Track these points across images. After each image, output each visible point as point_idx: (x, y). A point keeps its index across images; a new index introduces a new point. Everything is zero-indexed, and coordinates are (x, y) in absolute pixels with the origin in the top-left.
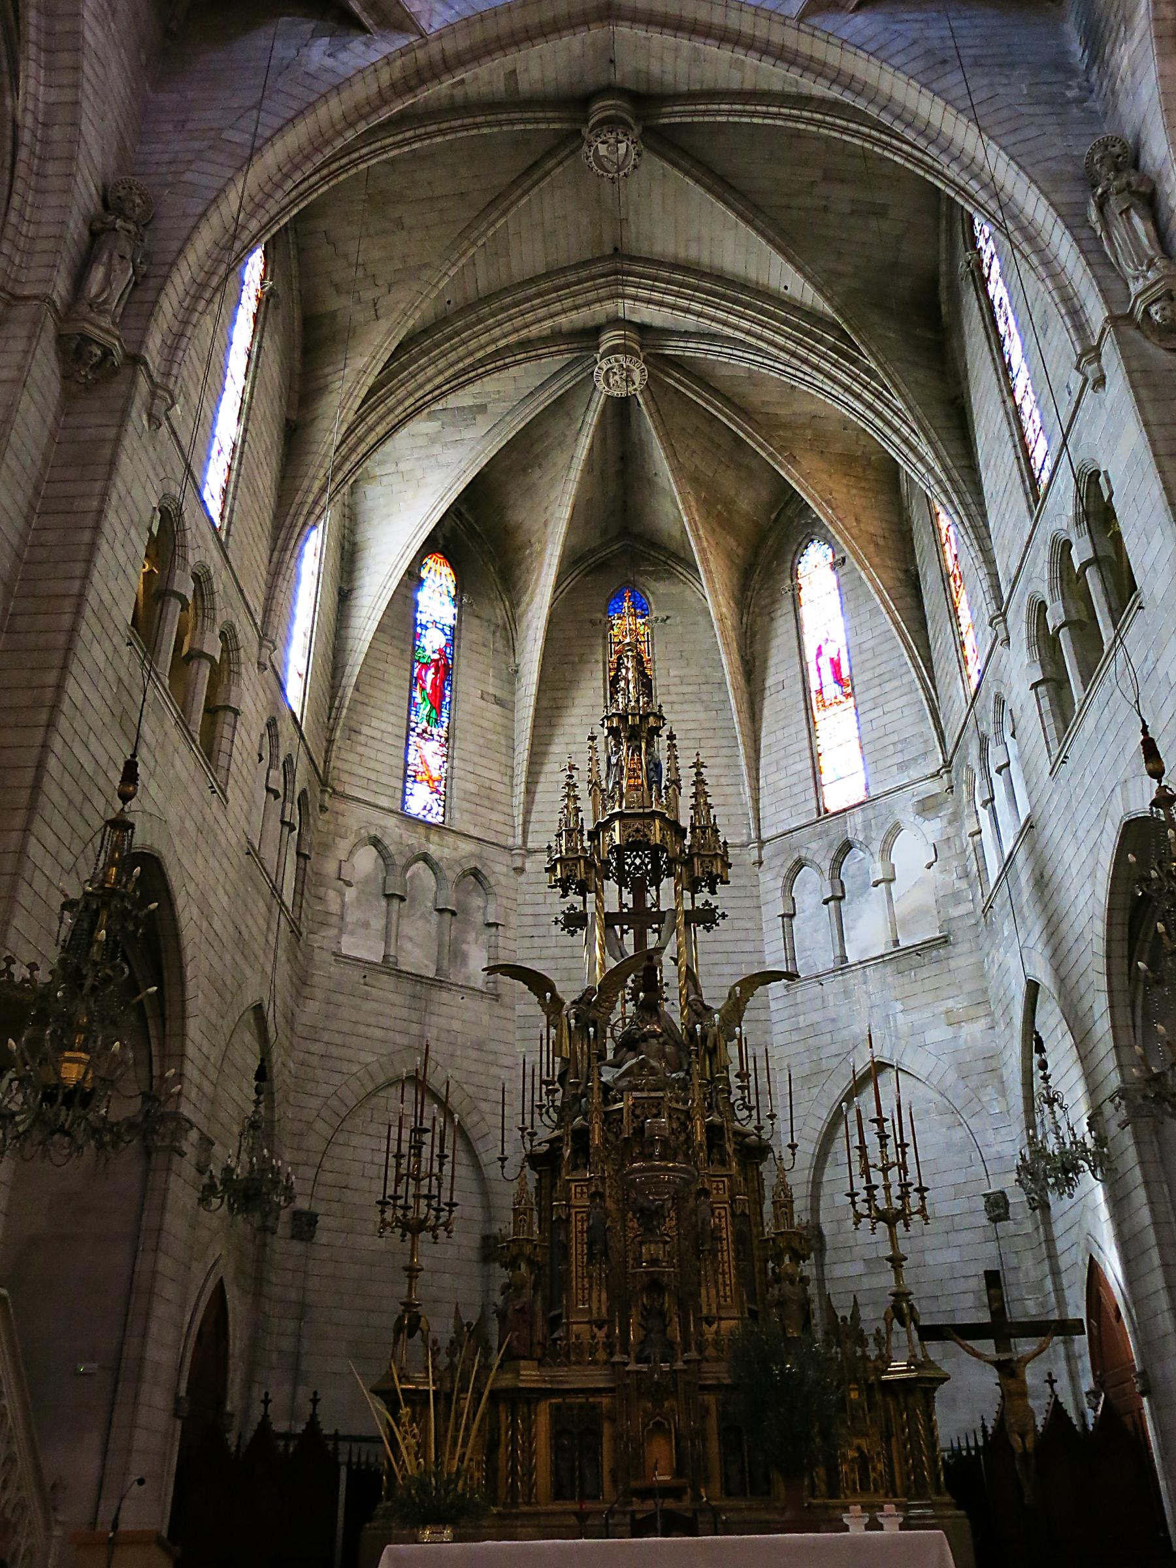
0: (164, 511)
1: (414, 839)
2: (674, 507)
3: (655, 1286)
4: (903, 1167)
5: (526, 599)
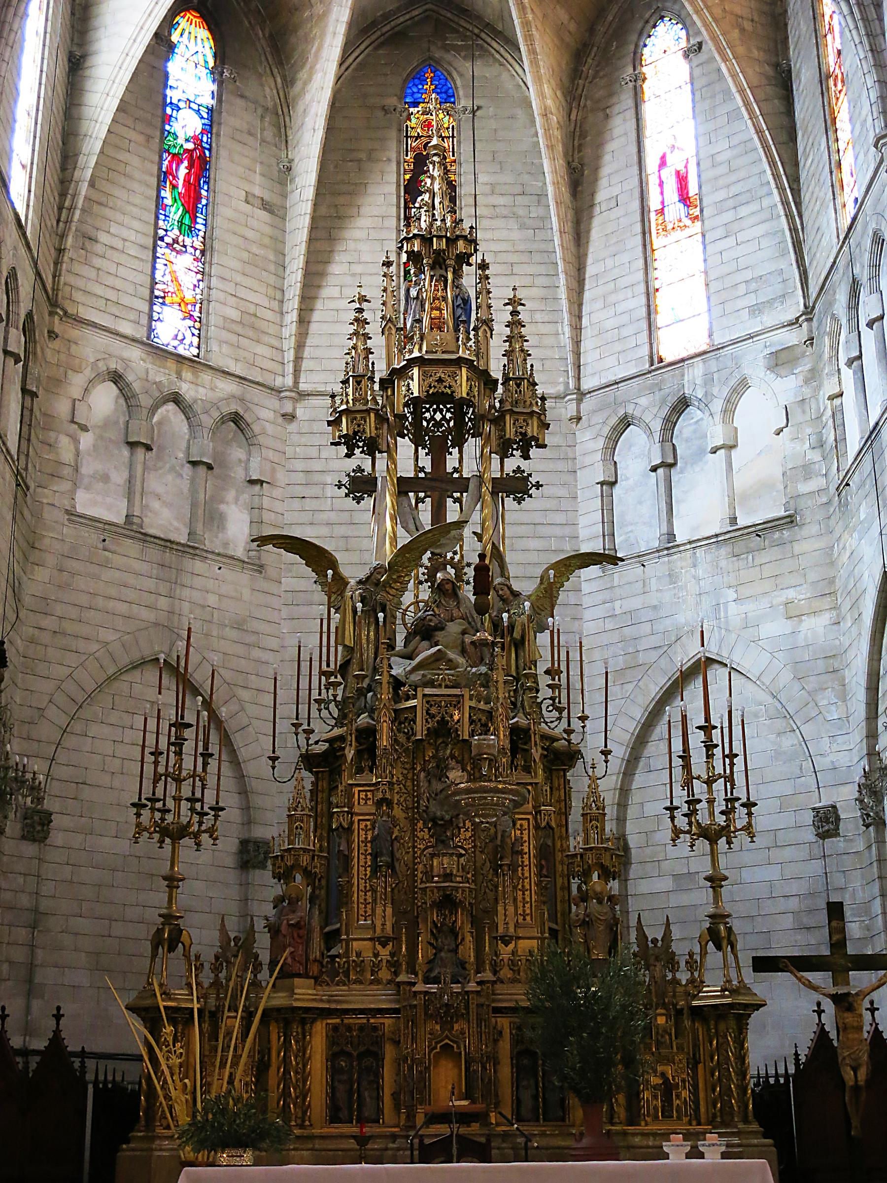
1: (163, 375)
3: (447, 902)
4: (730, 779)
5: (303, 75)
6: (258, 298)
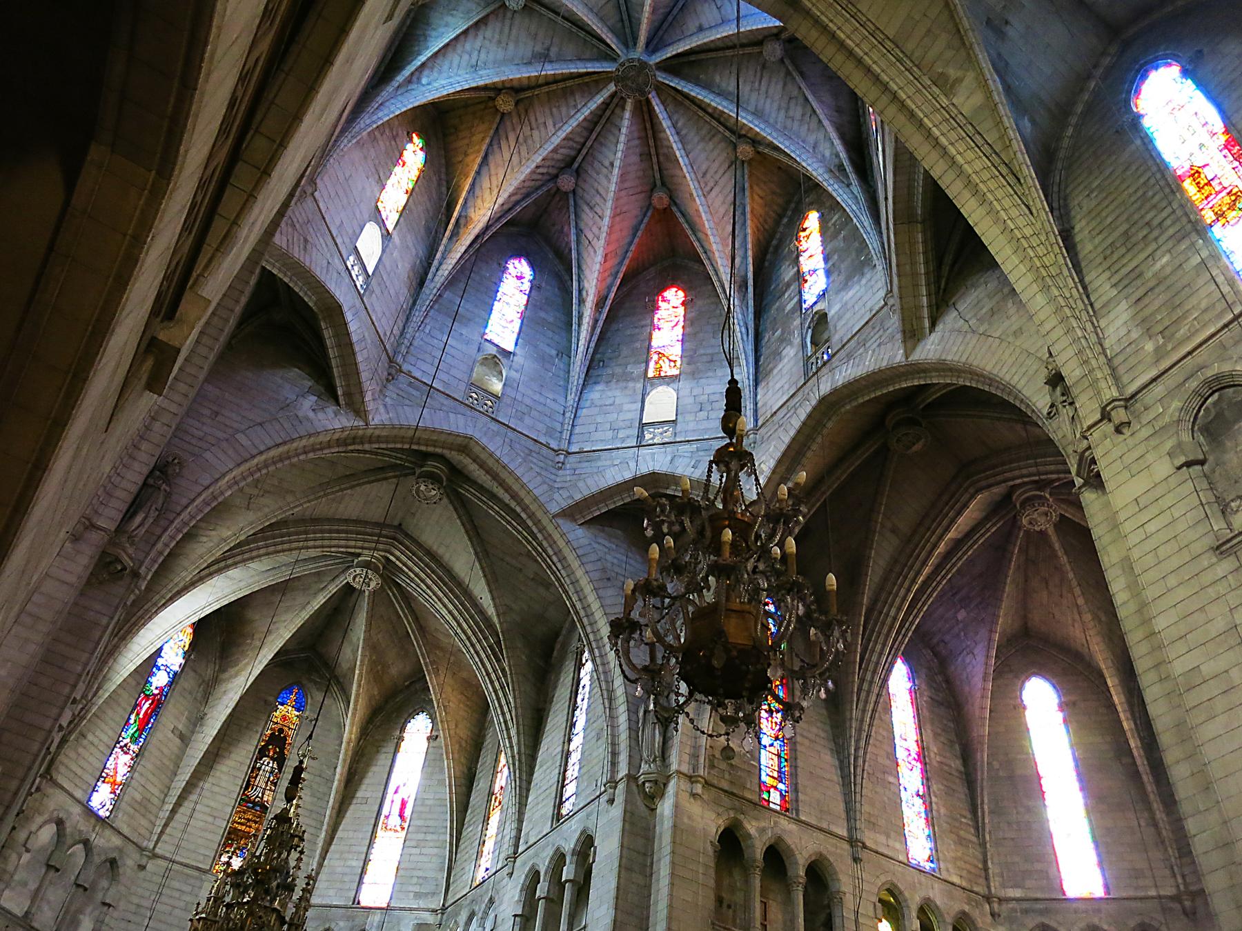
1: (84, 826)
2: (354, 649)
5: (232, 671)
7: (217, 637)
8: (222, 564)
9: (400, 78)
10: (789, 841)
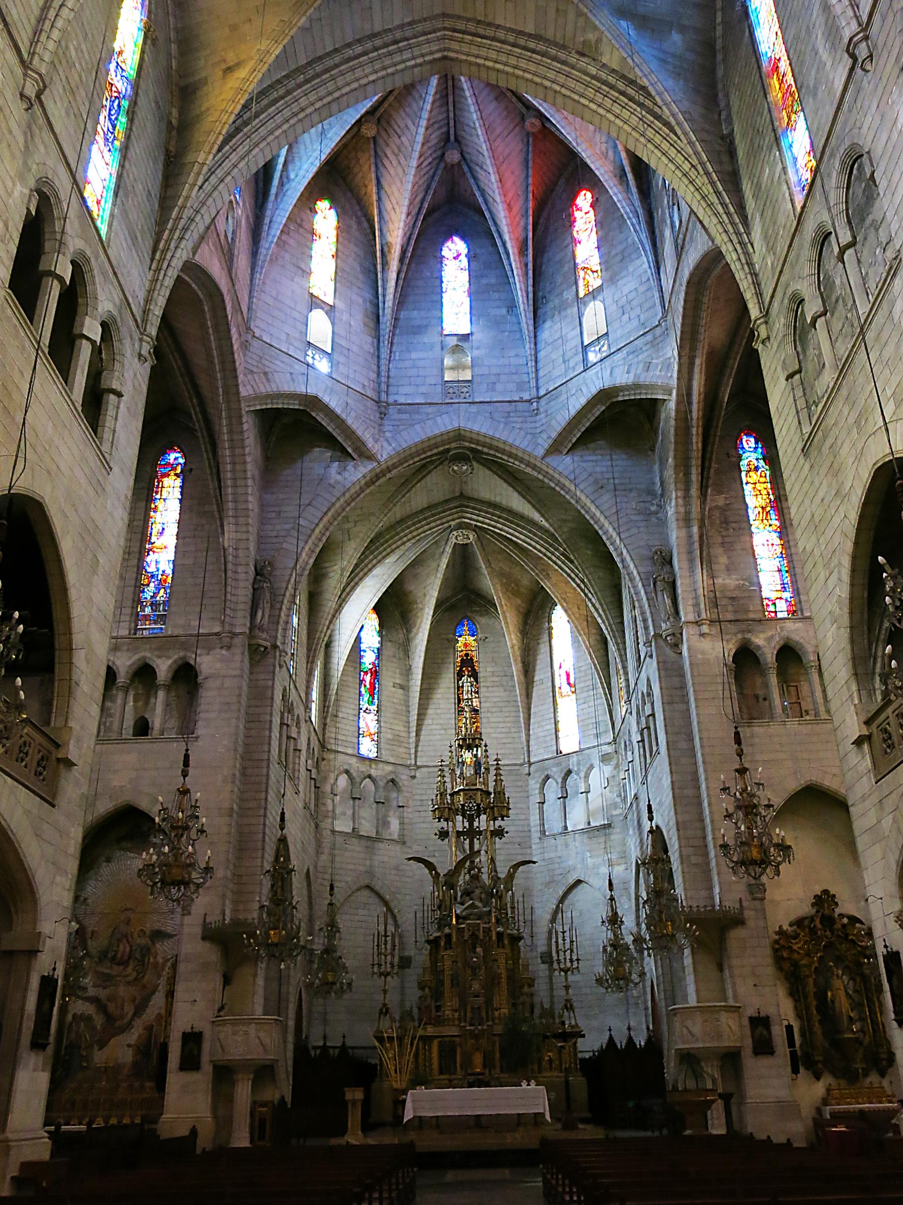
0: (39, 192)
1: (364, 768)
2: (489, 584)
4: (572, 951)
5: (414, 630)
6: (400, 728)
7: (393, 609)
8: (352, 584)
9: (273, 190)
10: (796, 637)
